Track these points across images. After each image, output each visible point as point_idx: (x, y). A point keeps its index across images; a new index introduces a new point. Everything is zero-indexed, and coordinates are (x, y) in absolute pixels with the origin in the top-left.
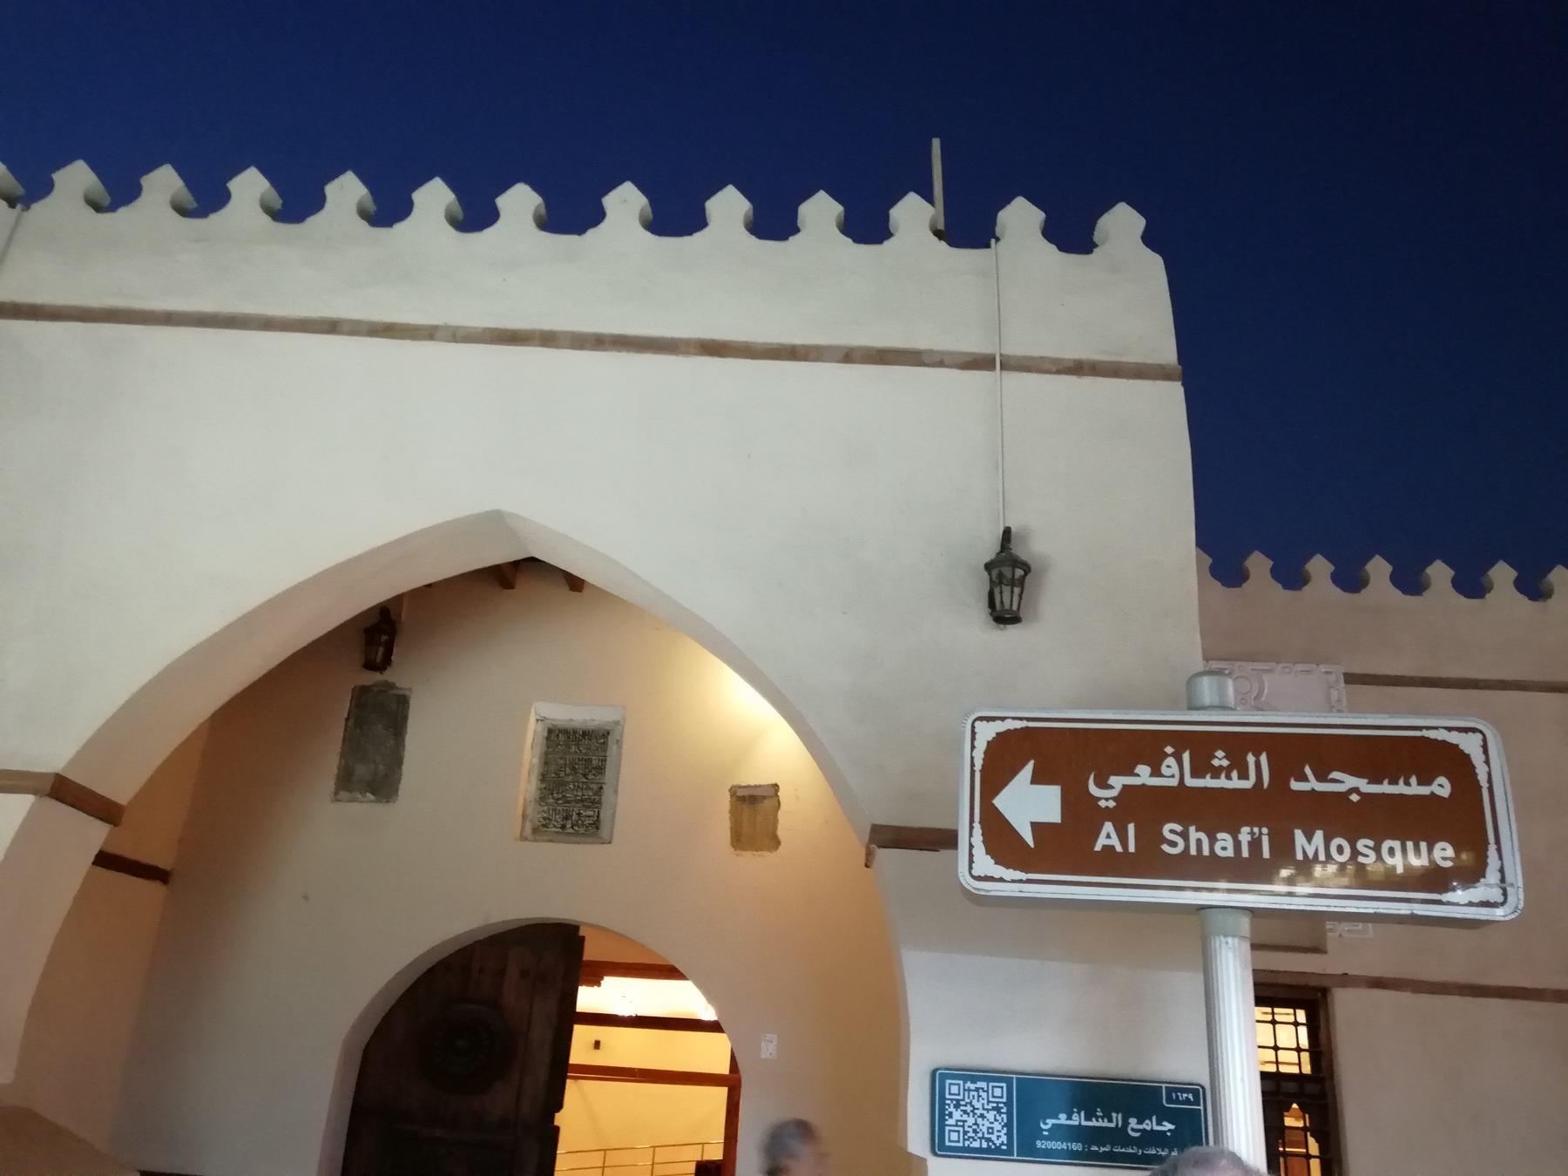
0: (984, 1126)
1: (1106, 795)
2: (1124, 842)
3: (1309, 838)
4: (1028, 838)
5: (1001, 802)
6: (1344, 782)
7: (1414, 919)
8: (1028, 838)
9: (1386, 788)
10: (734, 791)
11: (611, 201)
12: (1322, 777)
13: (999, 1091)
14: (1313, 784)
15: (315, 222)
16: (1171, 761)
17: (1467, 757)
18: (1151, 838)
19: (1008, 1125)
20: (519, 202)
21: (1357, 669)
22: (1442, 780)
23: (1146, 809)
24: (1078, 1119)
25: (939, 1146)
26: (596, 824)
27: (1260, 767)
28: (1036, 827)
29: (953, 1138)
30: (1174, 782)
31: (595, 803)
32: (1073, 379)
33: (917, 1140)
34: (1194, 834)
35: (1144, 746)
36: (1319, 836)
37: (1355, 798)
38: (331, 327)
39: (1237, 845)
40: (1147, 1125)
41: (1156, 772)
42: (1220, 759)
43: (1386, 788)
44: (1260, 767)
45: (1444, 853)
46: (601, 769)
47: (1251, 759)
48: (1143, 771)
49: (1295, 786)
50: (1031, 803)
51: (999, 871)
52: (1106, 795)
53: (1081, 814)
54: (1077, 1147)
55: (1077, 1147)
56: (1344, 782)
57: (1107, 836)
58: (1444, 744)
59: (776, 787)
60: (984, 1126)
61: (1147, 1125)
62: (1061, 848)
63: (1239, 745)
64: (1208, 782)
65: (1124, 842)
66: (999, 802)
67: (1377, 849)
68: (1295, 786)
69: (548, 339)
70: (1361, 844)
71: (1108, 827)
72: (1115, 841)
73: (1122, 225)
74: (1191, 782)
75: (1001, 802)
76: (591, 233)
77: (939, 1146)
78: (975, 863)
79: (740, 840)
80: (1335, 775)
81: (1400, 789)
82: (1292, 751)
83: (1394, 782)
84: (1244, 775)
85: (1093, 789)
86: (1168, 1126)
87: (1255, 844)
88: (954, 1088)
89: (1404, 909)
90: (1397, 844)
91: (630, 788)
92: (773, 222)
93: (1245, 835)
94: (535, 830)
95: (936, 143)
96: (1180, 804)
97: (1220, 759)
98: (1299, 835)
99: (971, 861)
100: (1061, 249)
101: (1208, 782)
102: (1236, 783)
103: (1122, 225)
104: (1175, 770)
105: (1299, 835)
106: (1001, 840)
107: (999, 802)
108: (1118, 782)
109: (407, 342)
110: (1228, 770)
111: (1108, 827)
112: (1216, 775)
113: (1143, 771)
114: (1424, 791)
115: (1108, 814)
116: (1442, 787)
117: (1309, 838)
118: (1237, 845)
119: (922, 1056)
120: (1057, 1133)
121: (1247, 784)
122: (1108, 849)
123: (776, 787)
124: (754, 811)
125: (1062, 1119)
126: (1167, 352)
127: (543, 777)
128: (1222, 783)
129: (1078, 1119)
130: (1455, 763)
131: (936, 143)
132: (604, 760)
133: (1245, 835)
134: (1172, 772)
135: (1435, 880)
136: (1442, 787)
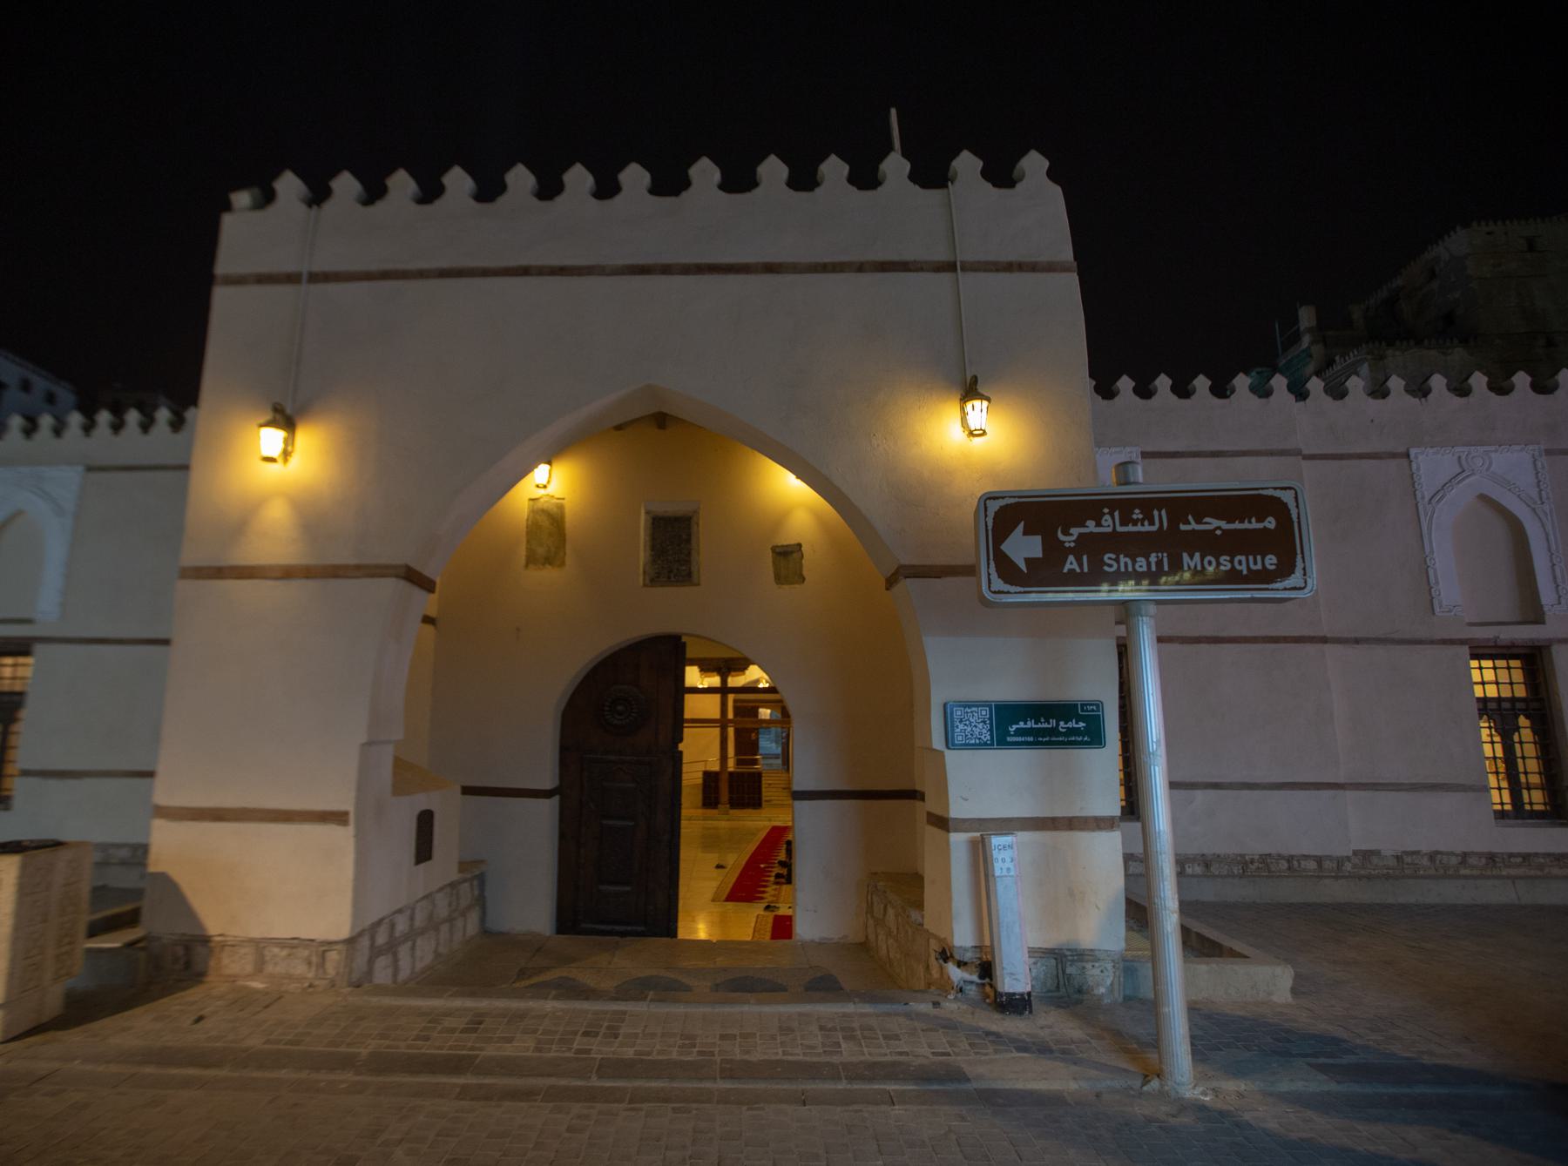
0: (977, 731)
1: (1069, 540)
2: (1081, 565)
3: (1192, 557)
4: (1023, 567)
5: (1006, 547)
6: (1212, 523)
7: (1253, 600)
8: (1023, 567)
9: (1237, 525)
10: (774, 549)
11: (694, 172)
12: (1198, 522)
13: (985, 712)
14: (1194, 526)
15: (502, 200)
16: (1107, 517)
17: (1285, 505)
18: (1097, 564)
19: (991, 730)
20: (635, 177)
21: (1149, 449)
22: (1271, 519)
23: (1093, 546)
24: (1030, 724)
25: (949, 743)
26: (690, 575)
27: (1161, 518)
28: (1027, 560)
29: (959, 739)
30: (1110, 530)
31: (688, 562)
32: (1007, 275)
33: (938, 742)
34: (1123, 559)
35: (1089, 508)
36: (1197, 556)
37: (1218, 532)
38: (525, 271)
39: (1149, 564)
40: (1070, 725)
41: (1099, 524)
42: (1137, 514)
43: (1237, 525)
44: (1161, 518)
45: (1271, 561)
46: (688, 541)
47: (1156, 513)
48: (1091, 524)
49: (1183, 527)
50: (1024, 547)
51: (1007, 587)
52: (1069, 540)
53: (1055, 553)
54: (1031, 739)
55: (1031, 739)
56: (1212, 523)
57: (1071, 564)
58: (1272, 498)
59: (800, 545)
60: (977, 731)
61: (1070, 725)
62: (1044, 572)
63: (1148, 505)
64: (1130, 528)
65: (1081, 565)
66: (1004, 547)
67: (1232, 561)
68: (1183, 527)
69: (666, 270)
70: (1223, 559)
71: (1071, 558)
72: (1075, 566)
73: (1034, 164)
74: (1120, 529)
75: (1006, 547)
76: (684, 194)
77: (949, 743)
78: (989, 580)
79: (780, 579)
80: (1207, 519)
81: (1246, 525)
82: (1181, 506)
83: (1242, 522)
84: (1152, 523)
85: (1061, 537)
86: (1082, 724)
87: (1159, 563)
88: (958, 713)
89: (1248, 595)
90: (1243, 558)
91: (707, 548)
92: (739, 180)
93: (1153, 558)
94: (652, 580)
95: (893, 111)
96: (1115, 542)
97: (1137, 514)
98: (1185, 556)
99: (1295, 589)
100: (995, 185)
101: (1130, 528)
102: (1147, 528)
103: (1034, 164)
104: (1110, 522)
105: (1185, 556)
106: (1007, 569)
107: (1004, 547)
108: (1075, 531)
109: (575, 278)
110: (1142, 521)
111: (1071, 558)
112: (1135, 523)
113: (1091, 524)
114: (1260, 526)
115: (1071, 551)
116: (1270, 523)
117: (1192, 557)
118: (1149, 564)
119: (938, 697)
120: (1019, 732)
121: (1155, 528)
122: (1072, 571)
123: (800, 545)
124: (787, 558)
125: (1022, 725)
126: (1067, 254)
127: (653, 548)
128: (1139, 528)
129: (1030, 724)
130: (1277, 507)
131: (893, 111)
132: (689, 535)
133: (1153, 558)
134: (1109, 524)
135: (1265, 577)
136: (1270, 523)
